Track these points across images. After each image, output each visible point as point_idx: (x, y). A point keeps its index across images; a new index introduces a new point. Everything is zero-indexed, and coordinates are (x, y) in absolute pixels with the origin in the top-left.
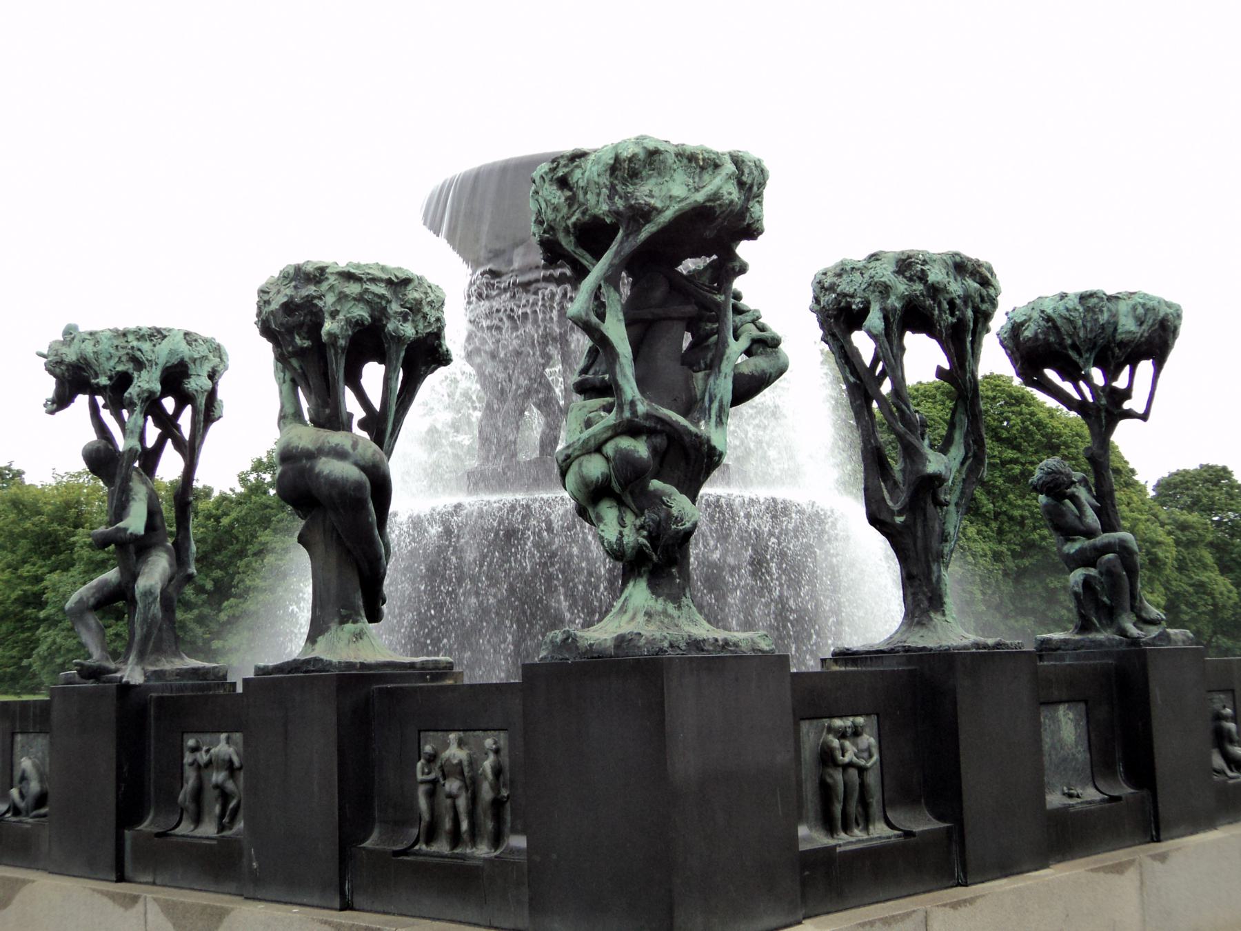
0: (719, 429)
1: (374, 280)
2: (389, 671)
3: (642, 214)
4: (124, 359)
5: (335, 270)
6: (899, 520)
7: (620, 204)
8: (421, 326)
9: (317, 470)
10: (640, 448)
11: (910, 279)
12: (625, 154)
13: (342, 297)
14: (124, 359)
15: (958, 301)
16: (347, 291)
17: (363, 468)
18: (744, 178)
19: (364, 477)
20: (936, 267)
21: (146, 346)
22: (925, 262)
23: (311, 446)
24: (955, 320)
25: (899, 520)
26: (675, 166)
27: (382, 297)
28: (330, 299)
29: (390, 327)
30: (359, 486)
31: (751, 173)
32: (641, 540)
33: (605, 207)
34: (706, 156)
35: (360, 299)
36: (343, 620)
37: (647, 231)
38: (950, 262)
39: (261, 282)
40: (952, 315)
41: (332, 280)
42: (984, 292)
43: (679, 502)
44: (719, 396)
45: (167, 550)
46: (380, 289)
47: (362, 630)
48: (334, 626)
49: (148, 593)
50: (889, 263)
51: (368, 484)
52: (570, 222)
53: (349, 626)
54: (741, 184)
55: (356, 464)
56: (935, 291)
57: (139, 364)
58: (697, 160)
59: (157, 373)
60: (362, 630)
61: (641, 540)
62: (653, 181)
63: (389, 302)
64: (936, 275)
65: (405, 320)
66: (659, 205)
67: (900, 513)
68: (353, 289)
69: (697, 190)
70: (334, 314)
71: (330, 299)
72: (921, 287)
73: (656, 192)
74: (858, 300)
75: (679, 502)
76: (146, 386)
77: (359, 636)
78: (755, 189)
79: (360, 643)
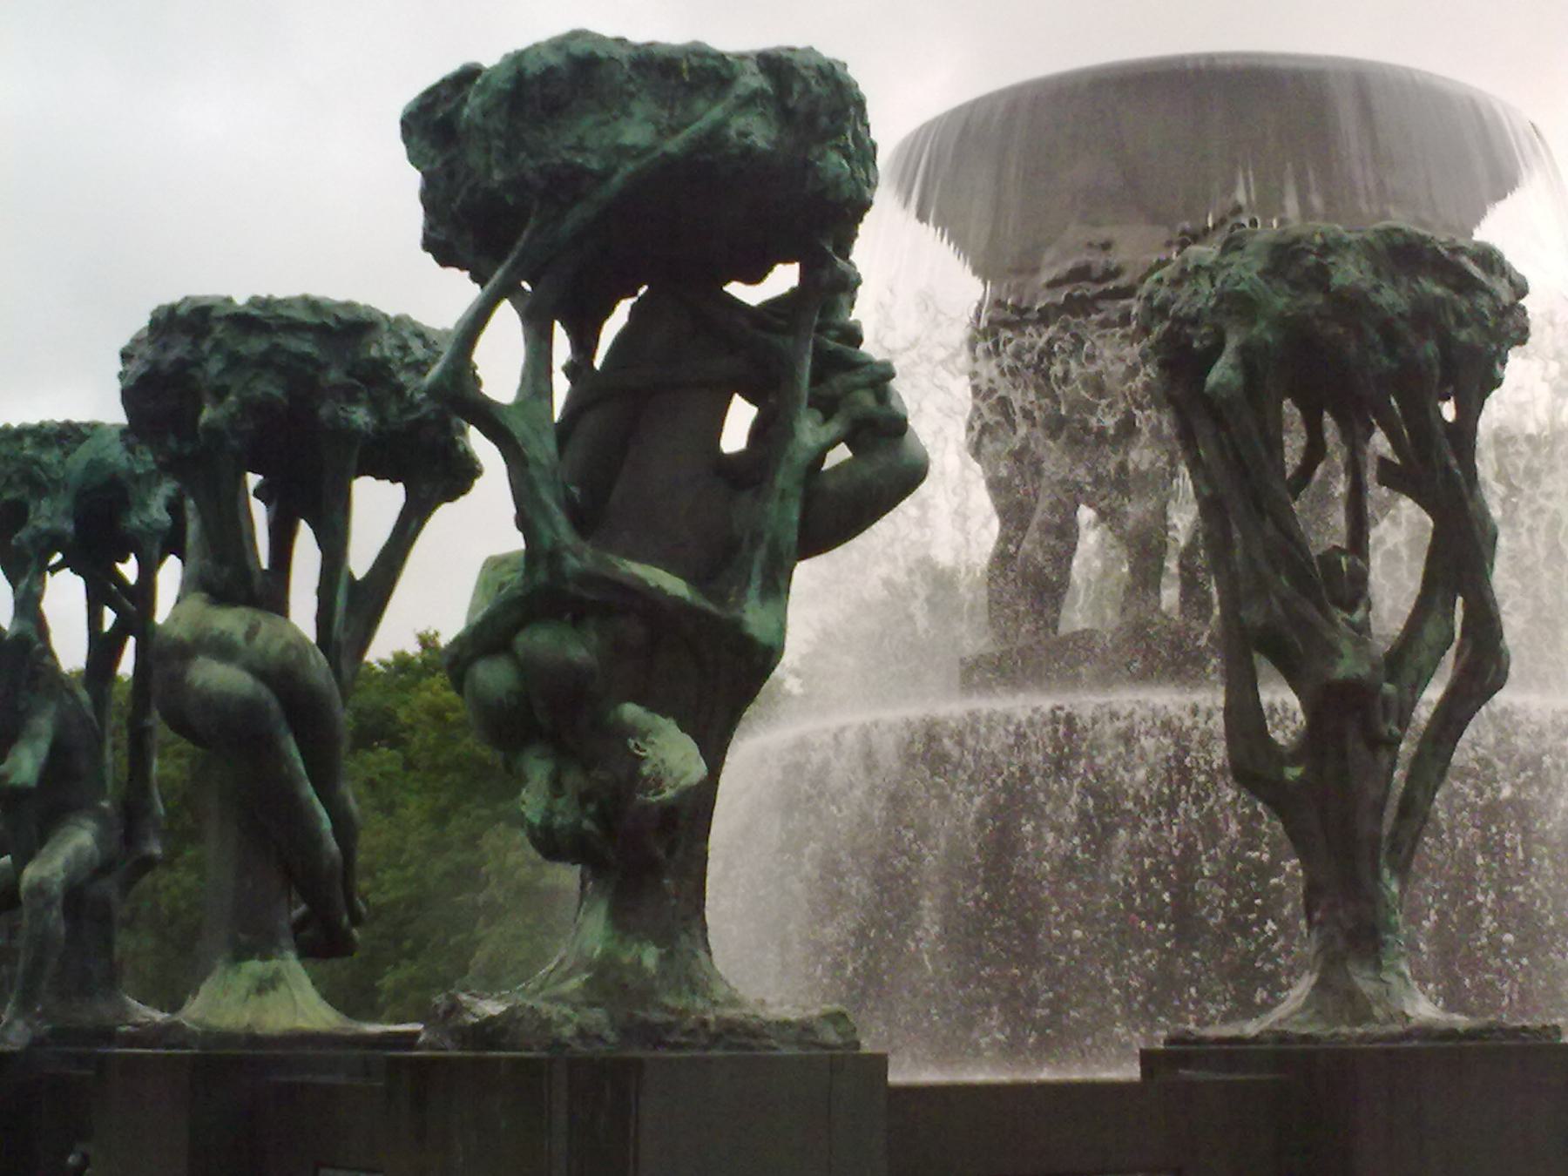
0: (770, 604)
1: (293, 327)
2: (310, 1051)
3: (567, 184)
4: (16, 478)
5: (222, 313)
6: (1293, 773)
7: (528, 165)
8: (393, 409)
9: (188, 679)
10: (576, 649)
11: (1294, 285)
12: (532, 68)
13: (235, 361)
14: (16, 478)
15: (1401, 325)
16: (242, 349)
17: (261, 673)
18: (791, 103)
19: (265, 692)
20: (1350, 257)
21: (51, 456)
22: (1326, 249)
23: (186, 636)
24: (1395, 366)
25: (1293, 773)
26: (631, 87)
27: (305, 358)
28: (215, 366)
29: (324, 412)
30: (250, 708)
31: (807, 89)
32: (587, 824)
33: (498, 176)
34: (695, 61)
35: (264, 362)
36: (240, 955)
37: (577, 215)
38: (1380, 246)
39: (124, 341)
40: (1391, 354)
41: (219, 330)
42: (1464, 305)
43: (673, 752)
44: (768, 536)
45: (101, 817)
46: (305, 345)
47: (277, 972)
48: (220, 967)
49: (39, 890)
50: (1256, 254)
51: (274, 705)
52: (455, 206)
53: (254, 966)
54: (786, 115)
55: (250, 668)
56: (1351, 305)
57: (39, 488)
58: (679, 73)
59: (64, 502)
60: (277, 972)
61: (587, 824)
62: (589, 120)
63: (322, 367)
64: (1349, 272)
65: (352, 399)
66: (595, 164)
67: (1295, 759)
68: (256, 345)
69: (675, 131)
70: (220, 394)
71: (215, 366)
72: (1319, 300)
73: (591, 141)
74: (1204, 330)
75: (673, 752)
76: (44, 525)
77: (265, 986)
78: (824, 121)
79: (270, 998)
